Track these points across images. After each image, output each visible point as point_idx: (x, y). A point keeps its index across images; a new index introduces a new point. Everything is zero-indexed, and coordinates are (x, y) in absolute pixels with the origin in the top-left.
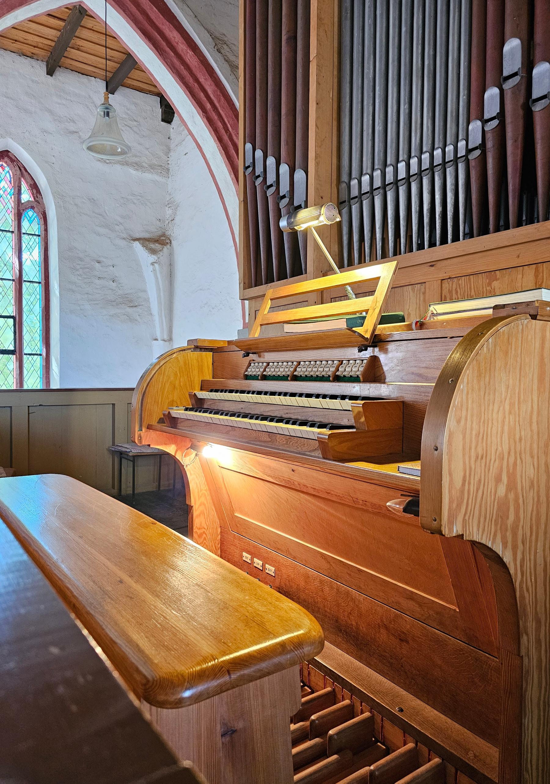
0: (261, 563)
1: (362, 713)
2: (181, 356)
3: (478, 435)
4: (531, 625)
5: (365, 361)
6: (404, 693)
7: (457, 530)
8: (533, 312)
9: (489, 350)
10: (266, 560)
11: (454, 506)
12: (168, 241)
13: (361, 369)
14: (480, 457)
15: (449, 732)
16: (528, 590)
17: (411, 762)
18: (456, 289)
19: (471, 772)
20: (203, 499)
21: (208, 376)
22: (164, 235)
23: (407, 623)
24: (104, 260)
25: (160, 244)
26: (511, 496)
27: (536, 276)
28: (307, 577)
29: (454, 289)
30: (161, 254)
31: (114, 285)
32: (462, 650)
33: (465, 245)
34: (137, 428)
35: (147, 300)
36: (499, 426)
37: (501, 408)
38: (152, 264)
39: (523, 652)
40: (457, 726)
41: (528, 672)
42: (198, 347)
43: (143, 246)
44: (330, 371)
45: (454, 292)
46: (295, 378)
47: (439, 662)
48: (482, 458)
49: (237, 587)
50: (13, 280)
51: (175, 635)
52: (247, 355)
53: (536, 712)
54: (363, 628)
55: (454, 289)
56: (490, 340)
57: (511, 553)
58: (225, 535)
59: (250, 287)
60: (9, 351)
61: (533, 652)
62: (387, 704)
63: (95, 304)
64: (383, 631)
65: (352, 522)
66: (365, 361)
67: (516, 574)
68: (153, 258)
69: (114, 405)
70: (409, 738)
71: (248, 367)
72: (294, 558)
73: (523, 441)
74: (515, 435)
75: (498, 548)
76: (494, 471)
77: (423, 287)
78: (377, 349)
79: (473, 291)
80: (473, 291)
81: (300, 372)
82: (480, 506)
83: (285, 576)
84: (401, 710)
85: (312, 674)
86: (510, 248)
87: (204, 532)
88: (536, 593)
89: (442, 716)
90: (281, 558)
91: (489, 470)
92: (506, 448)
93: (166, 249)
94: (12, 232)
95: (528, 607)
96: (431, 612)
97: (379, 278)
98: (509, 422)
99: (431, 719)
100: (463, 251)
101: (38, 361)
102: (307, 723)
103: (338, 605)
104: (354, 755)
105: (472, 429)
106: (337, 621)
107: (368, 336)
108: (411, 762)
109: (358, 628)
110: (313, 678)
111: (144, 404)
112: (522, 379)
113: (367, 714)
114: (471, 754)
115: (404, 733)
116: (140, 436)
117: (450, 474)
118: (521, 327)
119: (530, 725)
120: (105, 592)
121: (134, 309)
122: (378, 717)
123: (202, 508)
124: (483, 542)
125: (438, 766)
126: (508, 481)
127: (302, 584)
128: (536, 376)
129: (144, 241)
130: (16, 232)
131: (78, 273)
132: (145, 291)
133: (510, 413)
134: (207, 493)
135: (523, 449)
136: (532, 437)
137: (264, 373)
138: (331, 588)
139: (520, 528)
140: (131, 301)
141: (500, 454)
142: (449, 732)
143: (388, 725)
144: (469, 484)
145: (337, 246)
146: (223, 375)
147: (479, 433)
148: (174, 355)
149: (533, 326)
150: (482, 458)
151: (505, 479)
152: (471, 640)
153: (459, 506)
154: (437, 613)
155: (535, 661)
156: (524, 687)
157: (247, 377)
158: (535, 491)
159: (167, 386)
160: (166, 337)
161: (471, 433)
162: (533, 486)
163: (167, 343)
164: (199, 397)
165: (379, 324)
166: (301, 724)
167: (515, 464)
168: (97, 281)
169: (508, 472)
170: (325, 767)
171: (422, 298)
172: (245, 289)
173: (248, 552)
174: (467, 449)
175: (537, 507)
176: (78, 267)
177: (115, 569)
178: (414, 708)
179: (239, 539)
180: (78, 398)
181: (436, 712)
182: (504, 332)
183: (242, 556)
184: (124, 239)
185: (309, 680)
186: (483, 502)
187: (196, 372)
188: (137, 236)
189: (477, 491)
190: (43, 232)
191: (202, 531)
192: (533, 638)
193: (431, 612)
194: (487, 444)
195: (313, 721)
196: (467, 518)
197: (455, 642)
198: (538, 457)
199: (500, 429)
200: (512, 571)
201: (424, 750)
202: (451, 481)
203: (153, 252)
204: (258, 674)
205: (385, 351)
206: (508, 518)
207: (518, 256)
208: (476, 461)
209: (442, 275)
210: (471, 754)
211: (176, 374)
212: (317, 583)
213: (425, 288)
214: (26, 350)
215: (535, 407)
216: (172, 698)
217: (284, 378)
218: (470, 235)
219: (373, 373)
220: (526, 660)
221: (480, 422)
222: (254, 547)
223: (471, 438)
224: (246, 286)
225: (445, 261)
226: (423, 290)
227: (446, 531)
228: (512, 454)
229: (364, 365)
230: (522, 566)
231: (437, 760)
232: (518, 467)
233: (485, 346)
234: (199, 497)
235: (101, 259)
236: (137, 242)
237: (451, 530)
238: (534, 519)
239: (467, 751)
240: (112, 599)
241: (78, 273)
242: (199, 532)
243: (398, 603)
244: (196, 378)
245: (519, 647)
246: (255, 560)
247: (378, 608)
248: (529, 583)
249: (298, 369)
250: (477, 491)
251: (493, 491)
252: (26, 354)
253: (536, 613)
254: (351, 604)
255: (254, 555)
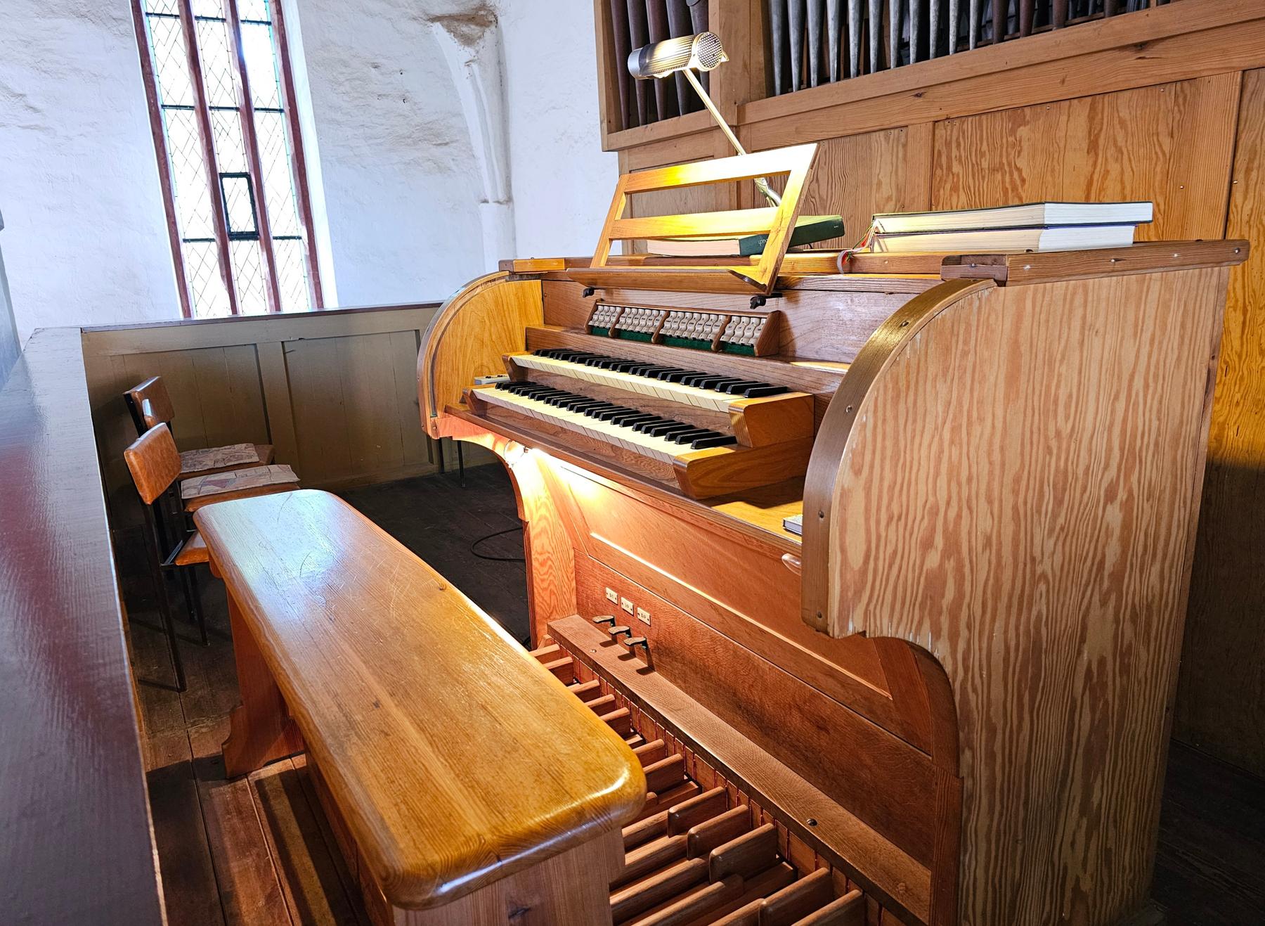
0: (631, 605)
1: (763, 822)
2: (488, 292)
3: (892, 488)
4: (979, 737)
5: (764, 321)
6: (823, 796)
7: (853, 627)
8: (999, 277)
9: (915, 352)
10: (637, 602)
11: (850, 594)
12: (491, 18)
13: (758, 334)
14: (896, 518)
15: (877, 854)
16: (975, 690)
17: (825, 891)
18: (958, 138)
19: (900, 912)
20: (543, 511)
21: (537, 323)
22: (483, 6)
23: (828, 704)
24: (384, 61)
25: (477, 24)
26: (950, 565)
27: (1091, 119)
28: (693, 631)
29: (954, 138)
30: (482, 44)
31: (406, 106)
32: (898, 748)
33: (976, 59)
34: (429, 412)
35: (465, 131)
36: (932, 466)
37: (936, 439)
38: (468, 64)
39: (964, 771)
40: (890, 846)
41: (971, 796)
42: (514, 272)
43: (450, 31)
44: (709, 332)
45: (954, 145)
46: (663, 340)
47: (869, 762)
48: (899, 518)
49: (540, 709)
50: (237, 109)
51: (435, 798)
52: (590, 292)
53: (983, 846)
54: (769, 707)
55: (954, 138)
56: (918, 336)
57: (948, 644)
58: (582, 562)
59: (620, 129)
60: (248, 233)
61: (982, 772)
62: (795, 814)
63: (377, 144)
64: (794, 712)
65: (746, 566)
66: (764, 321)
67: (955, 671)
68: (467, 53)
69: (417, 331)
70: (822, 861)
71: (593, 313)
72: (676, 603)
73: (975, 481)
74: (959, 474)
75: (926, 641)
76: (920, 531)
77: (903, 134)
78: (782, 301)
79: (985, 143)
80: (985, 143)
81: (670, 329)
82: (895, 588)
83: (664, 627)
84: (814, 823)
85: (699, 767)
86: (1048, 65)
87: (549, 558)
88: (989, 692)
89: (872, 831)
90: (659, 600)
91: (911, 534)
92: (942, 495)
93: (489, 34)
94: (224, 20)
95: (975, 713)
96: (858, 697)
97: (789, 172)
98: (950, 457)
99: (854, 836)
100: (971, 69)
101: (300, 248)
102: (684, 837)
103: (736, 673)
104: (746, 880)
105: (882, 479)
106: (735, 694)
107: (765, 280)
108: (825, 891)
109: (762, 707)
110: (699, 771)
111: (437, 370)
112: (977, 385)
113: (769, 826)
114: (901, 887)
115: (816, 853)
116: (435, 425)
117: (843, 550)
118: (977, 303)
119: (974, 863)
120: (352, 725)
121: (445, 148)
122: (784, 830)
123: (543, 524)
124: (900, 635)
125: (855, 901)
126: (945, 544)
127: (688, 639)
128: (1002, 377)
129: (449, 21)
130: (229, 19)
131: (342, 89)
132: (459, 115)
133: (952, 442)
134: (549, 502)
135: (974, 493)
136: (991, 473)
137: (617, 326)
138: (726, 649)
139: (965, 607)
140: (438, 135)
141: (931, 508)
142: (877, 854)
143: (795, 840)
144: (876, 559)
145: (761, 53)
146: (567, 307)
147: (895, 483)
148: (478, 290)
149: (1001, 298)
150: (899, 518)
151: (939, 541)
152: (910, 737)
153: (858, 593)
154: (866, 699)
155: (983, 779)
156: (964, 815)
157: (593, 331)
158: (994, 551)
159: (470, 342)
160: (502, 197)
161: (881, 485)
162: (991, 545)
163: (504, 207)
164: (519, 364)
165: (788, 252)
166: (677, 837)
167: (959, 516)
168: (377, 103)
169: (945, 531)
170: (703, 898)
171: (900, 155)
172: (610, 132)
173: (613, 588)
174: (874, 510)
175: (996, 572)
176: (342, 78)
177: (371, 680)
178: (832, 820)
179: (601, 568)
180: (359, 321)
181: (863, 825)
182: (943, 320)
183: (605, 593)
184: (415, 19)
185: (696, 774)
186: (901, 582)
187: (516, 315)
188: (437, 11)
189: (890, 566)
190: (276, 17)
191: (545, 556)
192: (981, 752)
193: (858, 697)
194: (908, 497)
195: (692, 836)
196: (871, 607)
197: (891, 737)
198: (1001, 501)
199: (932, 471)
200: (948, 669)
201: (841, 877)
202: (845, 562)
203: (468, 40)
204: (543, 856)
205: (794, 300)
206: (943, 596)
207: (1063, 82)
208: (888, 525)
209: (936, 114)
210: (901, 887)
211: (483, 322)
212: (707, 640)
213: (907, 136)
214: (275, 231)
215: (999, 425)
216: (419, 899)
217: (643, 338)
218: (981, 41)
219: (777, 342)
220: (968, 783)
221: (897, 466)
222: (621, 581)
223: (881, 491)
224: (613, 128)
225: (941, 88)
226: (903, 140)
227: (836, 631)
228: (954, 503)
229: (761, 327)
230: (965, 659)
231: (855, 892)
232: (963, 522)
233: (908, 348)
234: (537, 509)
235: (379, 61)
236: (438, 24)
237: (844, 627)
238: (989, 592)
239: (896, 881)
240: (359, 738)
241: (342, 89)
242: (541, 558)
243: (815, 679)
244: (517, 325)
245: (958, 766)
246: (623, 600)
247: (789, 683)
248: (978, 680)
249: (667, 325)
250: (890, 566)
251: (918, 562)
252: (276, 238)
253: (989, 718)
254: (753, 673)
255: (621, 593)
